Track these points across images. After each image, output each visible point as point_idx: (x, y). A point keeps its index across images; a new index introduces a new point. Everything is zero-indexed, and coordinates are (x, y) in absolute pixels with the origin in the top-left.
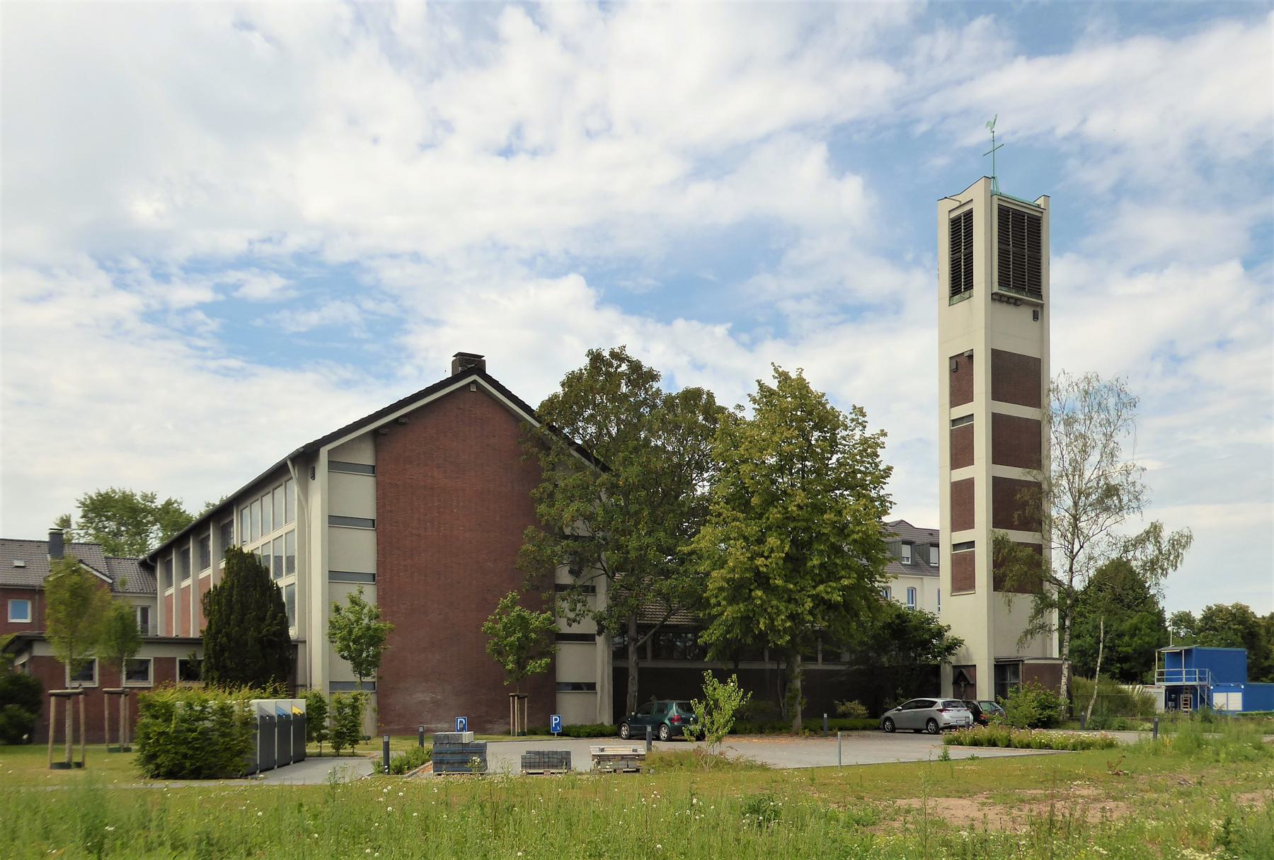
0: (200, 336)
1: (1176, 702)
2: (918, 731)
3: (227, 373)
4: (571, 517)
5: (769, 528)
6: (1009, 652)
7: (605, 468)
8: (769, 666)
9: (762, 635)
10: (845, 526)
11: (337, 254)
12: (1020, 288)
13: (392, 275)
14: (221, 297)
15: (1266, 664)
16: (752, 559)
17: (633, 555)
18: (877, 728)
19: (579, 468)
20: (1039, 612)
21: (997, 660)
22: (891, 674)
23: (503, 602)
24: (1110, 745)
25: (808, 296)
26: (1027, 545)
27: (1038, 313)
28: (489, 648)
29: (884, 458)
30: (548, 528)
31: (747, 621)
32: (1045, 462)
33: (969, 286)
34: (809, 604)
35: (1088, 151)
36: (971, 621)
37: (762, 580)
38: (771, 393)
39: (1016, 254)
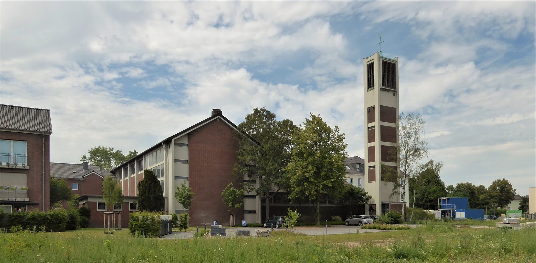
0: (115, 90)
1: (445, 215)
2: (357, 225)
3: (124, 103)
4: (248, 159)
5: (309, 163)
6: (386, 200)
7: (259, 144)
8: (311, 205)
9: (307, 197)
10: (332, 162)
11: (161, 61)
12: (389, 86)
13: (180, 69)
14: (121, 76)
15: (478, 202)
16: (304, 173)
17: (268, 172)
18: (344, 224)
19: (251, 144)
20: (395, 188)
21: (382, 203)
22: (349, 207)
23: (228, 186)
24: (408, 228)
25: (324, 75)
26: (391, 167)
27: (395, 93)
28: (224, 199)
29: (345, 141)
30: (241, 163)
31: (303, 192)
32: (397, 141)
33: (373, 86)
34: (321, 187)
35: (421, 25)
36: (374, 190)
37: (307, 179)
38: (310, 122)
39: (387, 76)
